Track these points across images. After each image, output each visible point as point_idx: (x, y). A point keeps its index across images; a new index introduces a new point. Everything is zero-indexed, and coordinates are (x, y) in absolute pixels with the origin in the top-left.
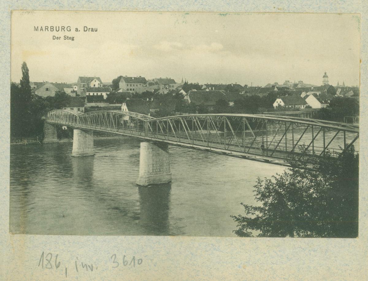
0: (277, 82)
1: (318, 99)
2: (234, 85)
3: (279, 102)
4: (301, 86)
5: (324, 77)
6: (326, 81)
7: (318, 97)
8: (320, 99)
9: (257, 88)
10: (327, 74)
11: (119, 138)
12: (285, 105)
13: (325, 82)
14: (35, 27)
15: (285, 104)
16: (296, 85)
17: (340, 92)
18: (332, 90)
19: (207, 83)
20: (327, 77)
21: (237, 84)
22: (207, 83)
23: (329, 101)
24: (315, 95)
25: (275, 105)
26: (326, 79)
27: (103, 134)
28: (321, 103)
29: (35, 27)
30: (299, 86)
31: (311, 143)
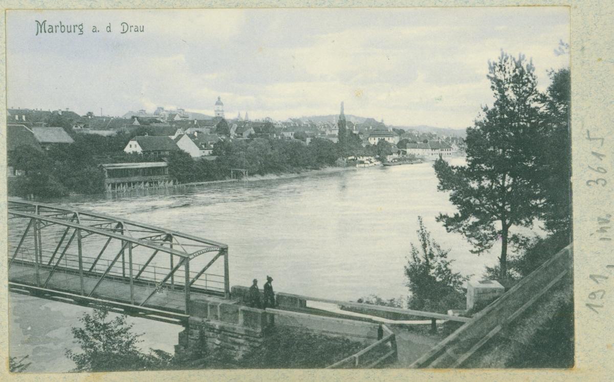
0: (144, 109)
1: (196, 143)
2: (62, 112)
3: (133, 147)
4: (181, 117)
5: (217, 104)
6: (220, 111)
7: (196, 139)
8: (199, 142)
9: (104, 120)
10: (221, 100)
11: (233, 326)
12: (143, 152)
13: (219, 112)
14: (79, 34)
15: (142, 149)
16: (172, 115)
17: (235, 129)
18: (222, 126)
19: (12, 108)
20: (222, 104)
21: (69, 110)
22: (41, 110)
23: (212, 146)
24: (192, 136)
25: (128, 149)
26: (220, 107)
27: (61, 270)
28: (201, 148)
29: (79, 34)
30: (177, 118)
31: (118, 256)
